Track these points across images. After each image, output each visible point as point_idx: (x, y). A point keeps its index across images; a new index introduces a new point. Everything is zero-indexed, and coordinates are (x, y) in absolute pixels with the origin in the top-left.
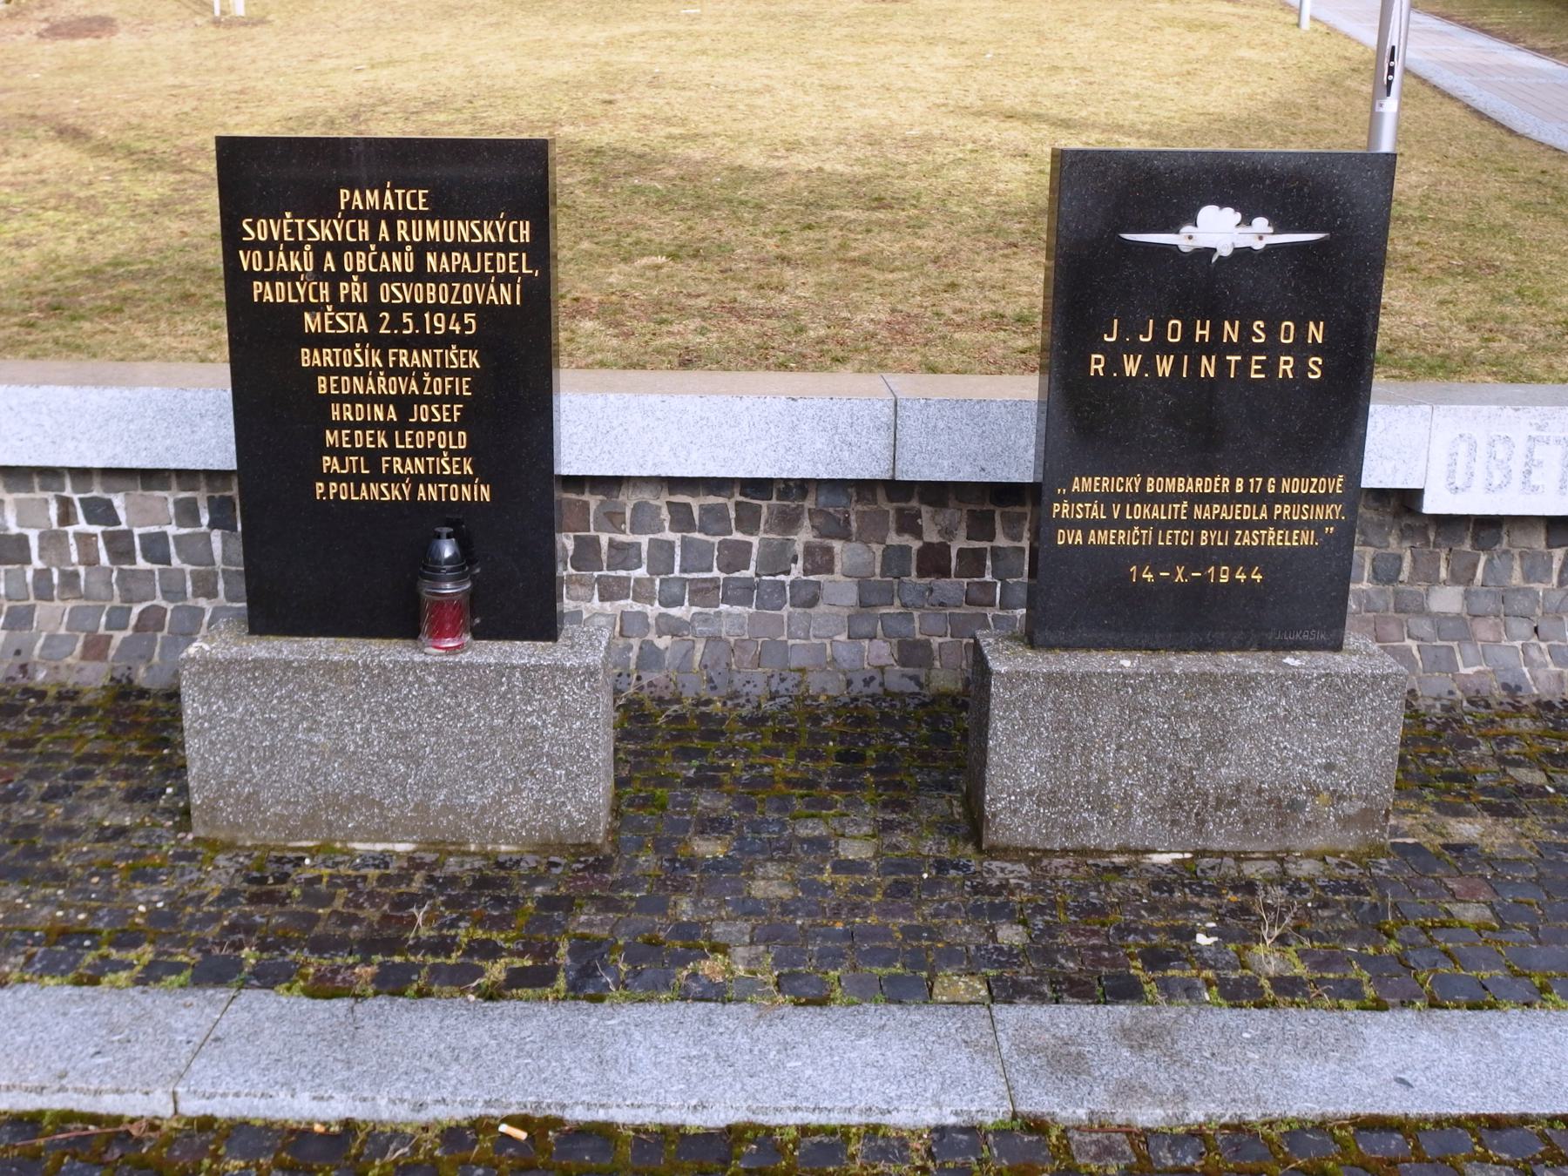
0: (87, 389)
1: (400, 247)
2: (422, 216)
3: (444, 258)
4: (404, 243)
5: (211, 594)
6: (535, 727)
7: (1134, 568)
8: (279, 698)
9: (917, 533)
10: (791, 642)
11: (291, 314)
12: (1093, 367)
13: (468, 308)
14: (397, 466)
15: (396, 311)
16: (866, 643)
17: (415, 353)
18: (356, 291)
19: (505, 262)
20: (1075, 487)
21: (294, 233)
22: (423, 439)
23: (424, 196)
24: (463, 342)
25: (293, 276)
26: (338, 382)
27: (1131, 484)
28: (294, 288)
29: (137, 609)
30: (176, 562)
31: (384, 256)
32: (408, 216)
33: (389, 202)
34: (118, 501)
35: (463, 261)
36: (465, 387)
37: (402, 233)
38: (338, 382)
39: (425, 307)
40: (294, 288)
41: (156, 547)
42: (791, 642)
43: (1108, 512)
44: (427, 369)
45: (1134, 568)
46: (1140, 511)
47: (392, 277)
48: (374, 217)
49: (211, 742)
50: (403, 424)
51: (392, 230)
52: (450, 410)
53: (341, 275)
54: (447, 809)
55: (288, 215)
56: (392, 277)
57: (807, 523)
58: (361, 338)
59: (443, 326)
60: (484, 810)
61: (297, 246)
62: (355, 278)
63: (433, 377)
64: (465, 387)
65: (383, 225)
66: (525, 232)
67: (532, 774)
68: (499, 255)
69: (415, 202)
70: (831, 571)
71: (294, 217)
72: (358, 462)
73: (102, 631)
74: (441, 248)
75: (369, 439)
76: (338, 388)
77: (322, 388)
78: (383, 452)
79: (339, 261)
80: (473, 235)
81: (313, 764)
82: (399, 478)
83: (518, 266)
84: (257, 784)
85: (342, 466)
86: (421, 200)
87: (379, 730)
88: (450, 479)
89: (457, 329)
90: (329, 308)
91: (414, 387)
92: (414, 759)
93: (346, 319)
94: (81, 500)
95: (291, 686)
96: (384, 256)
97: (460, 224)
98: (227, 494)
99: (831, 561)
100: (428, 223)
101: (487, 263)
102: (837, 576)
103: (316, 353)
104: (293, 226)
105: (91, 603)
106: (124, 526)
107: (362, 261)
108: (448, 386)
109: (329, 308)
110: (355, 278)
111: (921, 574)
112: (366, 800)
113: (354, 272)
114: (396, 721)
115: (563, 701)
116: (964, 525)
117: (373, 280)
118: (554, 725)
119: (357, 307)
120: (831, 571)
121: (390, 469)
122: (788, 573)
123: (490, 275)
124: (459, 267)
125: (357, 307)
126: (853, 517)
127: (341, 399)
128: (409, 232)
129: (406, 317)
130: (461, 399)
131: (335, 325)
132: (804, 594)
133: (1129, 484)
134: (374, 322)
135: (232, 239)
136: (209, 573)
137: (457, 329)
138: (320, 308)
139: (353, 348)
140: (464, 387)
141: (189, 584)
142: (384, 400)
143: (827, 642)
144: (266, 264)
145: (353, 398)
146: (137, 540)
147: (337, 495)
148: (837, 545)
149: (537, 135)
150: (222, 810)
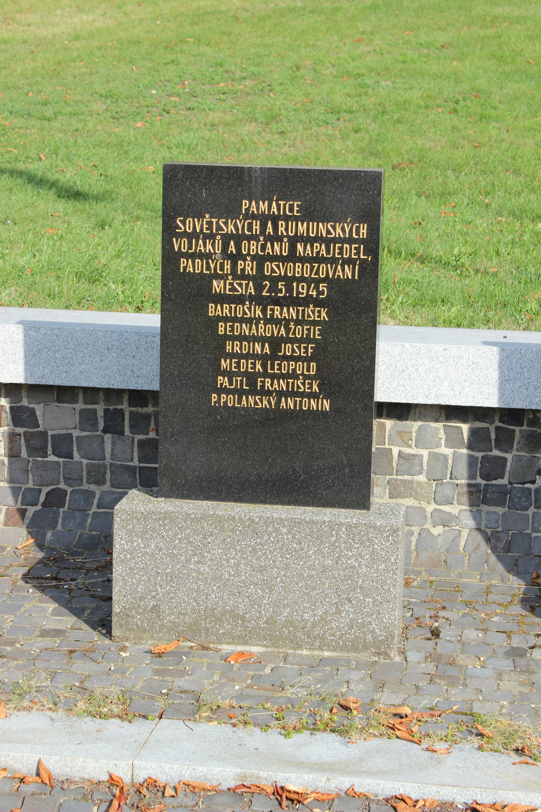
1: (280, 239)
2: (296, 219)
3: (308, 247)
4: (283, 236)
5: (100, 482)
6: (353, 567)
10: (534, 535)
14: (268, 384)
15: (274, 280)
17: (285, 310)
21: (210, 228)
22: (287, 367)
24: (318, 303)
25: (208, 256)
26: (232, 327)
28: (208, 263)
29: (45, 490)
30: (76, 455)
31: (269, 245)
32: (287, 219)
33: (274, 209)
34: (39, 410)
37: (281, 229)
38: (232, 327)
39: (294, 278)
40: (208, 263)
41: (63, 445)
42: (534, 535)
48: (264, 219)
49: (131, 568)
50: (273, 356)
51: (275, 227)
52: (306, 348)
54: (289, 623)
58: (251, 298)
59: (305, 291)
62: (249, 258)
65: (270, 224)
66: (364, 231)
67: (350, 601)
69: (291, 209)
71: (211, 217)
72: (242, 381)
74: (307, 240)
76: (232, 331)
77: (221, 331)
78: (259, 375)
79: (238, 247)
80: (328, 232)
82: (269, 393)
83: (358, 253)
86: (296, 209)
88: (303, 395)
89: (314, 294)
91: (283, 332)
93: (240, 285)
94: (131, 413)
95: (188, 531)
96: (269, 245)
98: (119, 407)
101: (337, 251)
104: (210, 223)
106: (41, 429)
107: (254, 248)
112: (235, 616)
113: (249, 254)
114: (258, 559)
117: (260, 260)
118: (367, 567)
119: (247, 278)
121: (263, 387)
122: (533, 482)
125: (247, 278)
128: (287, 229)
129: (280, 285)
130: (314, 341)
131: (233, 289)
134: (259, 288)
135: (169, 231)
136: (100, 465)
139: (244, 304)
140: (316, 333)
141: (85, 473)
142: (262, 340)
144: (190, 248)
145: (242, 338)
146: (50, 438)
147: (226, 403)
150: (133, 617)
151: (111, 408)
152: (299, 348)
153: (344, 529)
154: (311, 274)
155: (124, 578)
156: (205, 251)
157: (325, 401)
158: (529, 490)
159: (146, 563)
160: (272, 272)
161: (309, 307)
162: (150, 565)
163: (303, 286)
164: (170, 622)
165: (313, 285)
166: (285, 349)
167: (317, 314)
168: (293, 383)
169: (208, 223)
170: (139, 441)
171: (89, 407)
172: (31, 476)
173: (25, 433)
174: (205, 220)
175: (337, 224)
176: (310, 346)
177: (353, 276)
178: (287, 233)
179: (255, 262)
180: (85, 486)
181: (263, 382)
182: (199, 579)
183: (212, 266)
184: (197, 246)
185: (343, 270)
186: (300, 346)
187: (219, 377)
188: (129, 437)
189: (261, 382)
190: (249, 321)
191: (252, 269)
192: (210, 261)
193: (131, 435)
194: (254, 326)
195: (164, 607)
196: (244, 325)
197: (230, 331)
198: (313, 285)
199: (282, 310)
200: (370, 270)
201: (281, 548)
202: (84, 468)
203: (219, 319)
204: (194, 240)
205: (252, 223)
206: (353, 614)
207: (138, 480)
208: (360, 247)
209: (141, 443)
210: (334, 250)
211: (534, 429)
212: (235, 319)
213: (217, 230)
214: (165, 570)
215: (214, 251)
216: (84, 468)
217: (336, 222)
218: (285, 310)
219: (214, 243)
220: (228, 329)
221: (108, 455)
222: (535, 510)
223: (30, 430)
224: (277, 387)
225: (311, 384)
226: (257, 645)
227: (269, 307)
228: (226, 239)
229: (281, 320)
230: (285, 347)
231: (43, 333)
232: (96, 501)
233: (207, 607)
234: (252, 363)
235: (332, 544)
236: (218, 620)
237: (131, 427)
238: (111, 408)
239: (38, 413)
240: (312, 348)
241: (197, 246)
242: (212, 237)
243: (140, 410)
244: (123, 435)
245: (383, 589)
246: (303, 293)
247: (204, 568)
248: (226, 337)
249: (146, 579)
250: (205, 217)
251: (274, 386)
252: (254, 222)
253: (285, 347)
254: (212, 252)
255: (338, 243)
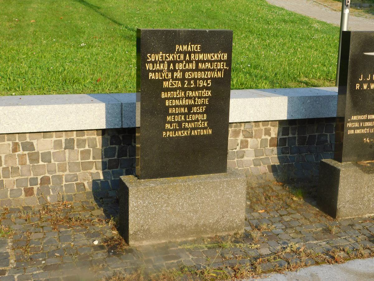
0: (32, 106)
1: (192, 62)
2: (198, 53)
3: (203, 65)
4: (193, 60)
6: (229, 198)
7: (365, 139)
8: (159, 198)
9: (270, 135)
10: (239, 169)
11: (159, 83)
12: (357, 87)
13: (209, 79)
14: (187, 125)
15: (189, 80)
16: (259, 167)
17: (194, 92)
18: (178, 75)
19: (220, 66)
20: (352, 119)
21: (162, 58)
22: (194, 117)
23: (199, 47)
24: (207, 88)
25: (161, 71)
26: (172, 102)
27: (364, 117)
28: (161, 74)
29: (39, 178)
31: (187, 64)
32: (195, 53)
33: (189, 49)
34: (35, 142)
35: (208, 65)
36: (207, 101)
37: (192, 57)
38: (172, 102)
39: (198, 79)
40: (161, 74)
42: (239, 169)
43: (360, 125)
44: (197, 97)
45: (365, 139)
46: (367, 124)
47: (188, 70)
48: (185, 53)
49: (137, 214)
50: (189, 113)
51: (190, 56)
52: (202, 108)
53: (175, 70)
55: (161, 53)
56: (188, 70)
57: (241, 134)
58: (179, 88)
59: (202, 84)
60: (214, 224)
61: (163, 62)
62: (179, 71)
63: (198, 99)
64: (207, 101)
65: (188, 55)
66: (226, 57)
67: (227, 212)
68: (218, 63)
69: (197, 49)
70: (247, 147)
71: (162, 53)
72: (176, 125)
73: (29, 186)
74: (203, 62)
75: (173, 118)
76: (172, 103)
77: (167, 104)
78: (183, 121)
79: (174, 66)
80: (212, 58)
81: (167, 217)
82: (187, 129)
83: (223, 66)
84: (150, 225)
85: (171, 127)
86: (198, 48)
87: (186, 204)
88: (201, 128)
89: (206, 85)
90: (171, 80)
91: (193, 102)
92: (196, 212)
93: (175, 83)
95: (162, 194)
96: (187, 64)
97: (208, 55)
98: (72, 137)
99: (248, 144)
100: (200, 54)
101: (215, 66)
102: (249, 149)
103: (166, 93)
104: (162, 56)
105: (23, 177)
106: (36, 151)
107: (180, 66)
108: (202, 101)
109: (171, 80)
110: (179, 71)
111: (270, 146)
112: (182, 226)
113: (179, 69)
114: (191, 201)
115: (237, 189)
116: (281, 132)
117: (184, 71)
118: (234, 197)
119: (178, 80)
120: (247, 147)
121: (184, 127)
122: (236, 149)
123: (222, 69)
124: (207, 67)
125: (178, 80)
126: (253, 132)
127: (172, 107)
128: (195, 57)
129: (192, 82)
130: (206, 105)
131: (172, 85)
132: (241, 155)
133: (364, 117)
134: (183, 84)
137: (206, 85)
138: (168, 80)
139: (176, 91)
141: (57, 168)
142: (184, 106)
143: (248, 167)
144: (153, 68)
145: (176, 106)
146: (40, 155)
147: (169, 135)
148: (249, 140)
149: (227, 29)
150: (139, 234)
151: (68, 138)
152: (199, 108)
153: (225, 183)
154: (204, 77)
155: (134, 219)
156: (160, 69)
157: (210, 130)
158: (235, 152)
159: (144, 210)
160: (188, 76)
161: (203, 90)
162: (146, 210)
163: (201, 82)
164: (155, 234)
165: (205, 81)
166: (194, 109)
167: (207, 93)
168: (197, 124)
169: (161, 56)
170: (81, 151)
171: (58, 139)
172: (32, 172)
173: (28, 154)
174: (160, 55)
175: (215, 54)
176: (204, 107)
177: (221, 76)
178: (195, 59)
179: (181, 73)
180: (57, 174)
181: (185, 125)
182: (167, 213)
183: (163, 76)
184: (156, 67)
185: (217, 74)
186: (200, 108)
187: (166, 124)
188: (76, 150)
189: (184, 124)
190: (179, 99)
191: (180, 76)
192: (162, 73)
193: (77, 149)
194: (181, 101)
195: (152, 228)
196: (177, 101)
197: (171, 104)
198: (205, 81)
199: (192, 93)
200: (228, 73)
201: (200, 195)
202: (57, 166)
203: (166, 99)
204: (155, 64)
205: (180, 55)
206: (228, 217)
207: (81, 168)
208: (224, 63)
209: (82, 152)
210: (214, 65)
211: (236, 129)
212: (173, 98)
213: (165, 59)
214: (152, 212)
215: (164, 68)
216: (57, 166)
217: (214, 53)
218: (194, 92)
219: (164, 65)
220: (170, 103)
221: (67, 159)
222: (237, 159)
223: (30, 152)
224: (190, 126)
225: (204, 124)
226: (191, 237)
227: (187, 92)
228: (169, 63)
229: (192, 97)
230: (194, 108)
231: (40, 108)
232: (64, 179)
233: (170, 225)
234: (173, 117)
235: (221, 190)
236: (175, 229)
237: (77, 145)
238: (68, 138)
239: (34, 144)
240: (205, 108)
241: (156, 67)
242: (163, 62)
243: (81, 138)
244: (74, 149)
245: (240, 205)
246: (201, 85)
247: (169, 208)
248: (169, 107)
249: (144, 217)
250: (160, 53)
251: (189, 126)
252: (225, 54)
253: (194, 108)
254: (163, 69)
255: (215, 62)
